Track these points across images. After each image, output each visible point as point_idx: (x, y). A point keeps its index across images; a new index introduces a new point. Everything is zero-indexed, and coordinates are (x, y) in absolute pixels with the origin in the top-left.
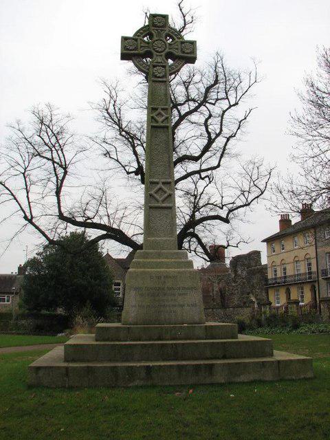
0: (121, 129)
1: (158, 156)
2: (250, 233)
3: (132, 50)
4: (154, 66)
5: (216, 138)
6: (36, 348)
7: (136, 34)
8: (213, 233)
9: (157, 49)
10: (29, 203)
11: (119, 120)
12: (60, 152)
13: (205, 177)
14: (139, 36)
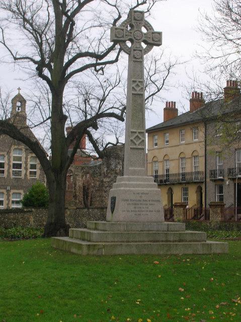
4: (134, 50)
13: (99, 70)
14: (124, 26)
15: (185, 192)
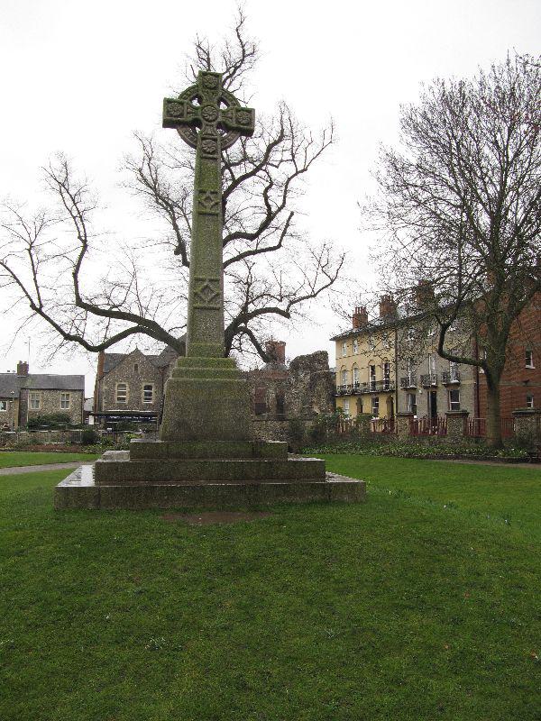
0: (157, 195)
1: (206, 239)
2: (310, 333)
3: (177, 115)
4: (203, 139)
5: (277, 212)
6: (60, 467)
7: (181, 96)
8: (268, 328)
9: (208, 114)
10: (37, 288)
11: (155, 183)
12: (78, 219)
15: (376, 403)
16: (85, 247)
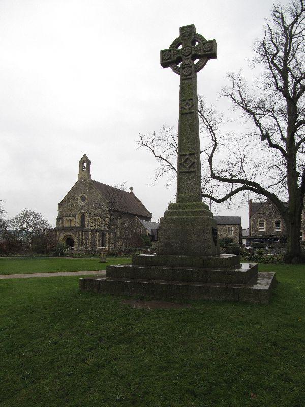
16: (216, 144)
